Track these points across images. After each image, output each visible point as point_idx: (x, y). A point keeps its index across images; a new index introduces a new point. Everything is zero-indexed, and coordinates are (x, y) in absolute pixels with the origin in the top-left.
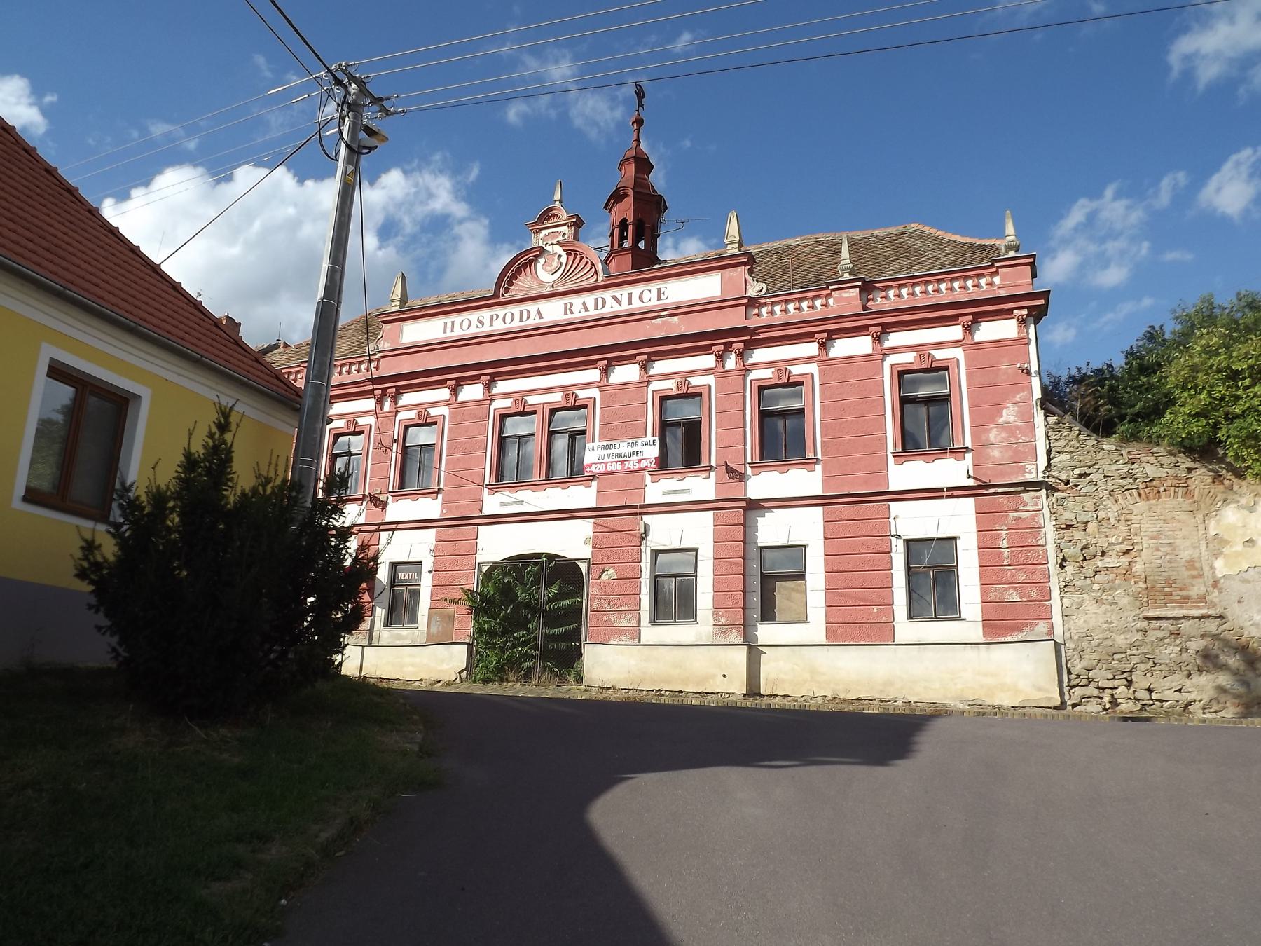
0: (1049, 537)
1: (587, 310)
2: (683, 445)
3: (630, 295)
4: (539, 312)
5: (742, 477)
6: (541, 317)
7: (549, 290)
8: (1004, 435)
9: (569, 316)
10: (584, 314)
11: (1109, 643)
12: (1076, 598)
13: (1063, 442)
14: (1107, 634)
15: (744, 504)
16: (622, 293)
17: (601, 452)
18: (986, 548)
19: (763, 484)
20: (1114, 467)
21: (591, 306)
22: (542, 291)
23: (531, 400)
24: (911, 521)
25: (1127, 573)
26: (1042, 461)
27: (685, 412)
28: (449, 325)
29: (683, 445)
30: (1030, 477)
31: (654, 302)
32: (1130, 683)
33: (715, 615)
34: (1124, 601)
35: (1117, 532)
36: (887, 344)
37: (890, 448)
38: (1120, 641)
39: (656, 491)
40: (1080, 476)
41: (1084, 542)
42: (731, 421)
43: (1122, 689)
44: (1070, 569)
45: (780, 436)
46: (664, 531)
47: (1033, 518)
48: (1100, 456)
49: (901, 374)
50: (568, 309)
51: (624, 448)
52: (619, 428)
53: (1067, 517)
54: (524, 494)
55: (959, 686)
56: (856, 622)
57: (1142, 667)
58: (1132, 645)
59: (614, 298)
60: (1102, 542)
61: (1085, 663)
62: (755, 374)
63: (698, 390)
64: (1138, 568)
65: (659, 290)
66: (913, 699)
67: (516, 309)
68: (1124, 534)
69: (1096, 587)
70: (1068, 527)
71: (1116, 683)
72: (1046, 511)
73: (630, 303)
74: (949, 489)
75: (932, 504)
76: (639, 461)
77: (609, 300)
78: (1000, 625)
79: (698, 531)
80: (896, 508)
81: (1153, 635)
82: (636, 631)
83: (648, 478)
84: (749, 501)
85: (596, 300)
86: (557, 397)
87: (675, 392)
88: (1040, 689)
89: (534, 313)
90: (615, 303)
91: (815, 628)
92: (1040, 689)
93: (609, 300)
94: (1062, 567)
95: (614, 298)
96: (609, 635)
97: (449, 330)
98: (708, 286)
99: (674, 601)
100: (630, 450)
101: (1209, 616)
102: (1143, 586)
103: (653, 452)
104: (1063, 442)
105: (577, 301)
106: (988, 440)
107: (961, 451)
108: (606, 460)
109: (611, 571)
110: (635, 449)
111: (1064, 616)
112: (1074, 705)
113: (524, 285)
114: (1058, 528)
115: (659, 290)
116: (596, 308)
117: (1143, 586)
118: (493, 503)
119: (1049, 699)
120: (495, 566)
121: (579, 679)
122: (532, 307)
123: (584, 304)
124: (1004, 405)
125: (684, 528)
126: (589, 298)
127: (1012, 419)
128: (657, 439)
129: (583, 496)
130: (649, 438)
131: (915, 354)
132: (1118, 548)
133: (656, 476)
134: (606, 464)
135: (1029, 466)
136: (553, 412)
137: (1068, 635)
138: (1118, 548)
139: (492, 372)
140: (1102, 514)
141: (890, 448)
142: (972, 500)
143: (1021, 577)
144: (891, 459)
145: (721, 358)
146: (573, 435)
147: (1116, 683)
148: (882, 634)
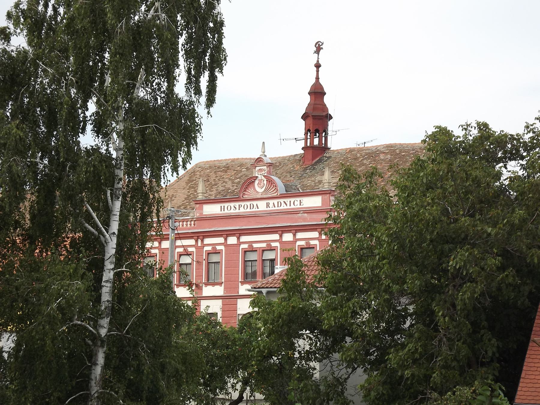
6: (258, 208)
9: (268, 209)
10: (274, 208)
16: (287, 200)
21: (276, 205)
22: (259, 196)
23: (255, 246)
28: (223, 208)
31: (299, 206)
36: (241, 241)
49: (208, 254)
50: (268, 205)
59: (284, 202)
62: (299, 243)
63: (313, 246)
67: (248, 203)
77: (283, 203)
80: (239, 301)
86: (264, 245)
90: (285, 205)
93: (283, 203)
95: (284, 202)
97: (223, 210)
105: (271, 202)
113: (251, 192)
122: (255, 203)
126: (275, 201)
131: (266, 244)
136: (263, 251)
139: (239, 233)
142: (221, 300)
145: (320, 234)
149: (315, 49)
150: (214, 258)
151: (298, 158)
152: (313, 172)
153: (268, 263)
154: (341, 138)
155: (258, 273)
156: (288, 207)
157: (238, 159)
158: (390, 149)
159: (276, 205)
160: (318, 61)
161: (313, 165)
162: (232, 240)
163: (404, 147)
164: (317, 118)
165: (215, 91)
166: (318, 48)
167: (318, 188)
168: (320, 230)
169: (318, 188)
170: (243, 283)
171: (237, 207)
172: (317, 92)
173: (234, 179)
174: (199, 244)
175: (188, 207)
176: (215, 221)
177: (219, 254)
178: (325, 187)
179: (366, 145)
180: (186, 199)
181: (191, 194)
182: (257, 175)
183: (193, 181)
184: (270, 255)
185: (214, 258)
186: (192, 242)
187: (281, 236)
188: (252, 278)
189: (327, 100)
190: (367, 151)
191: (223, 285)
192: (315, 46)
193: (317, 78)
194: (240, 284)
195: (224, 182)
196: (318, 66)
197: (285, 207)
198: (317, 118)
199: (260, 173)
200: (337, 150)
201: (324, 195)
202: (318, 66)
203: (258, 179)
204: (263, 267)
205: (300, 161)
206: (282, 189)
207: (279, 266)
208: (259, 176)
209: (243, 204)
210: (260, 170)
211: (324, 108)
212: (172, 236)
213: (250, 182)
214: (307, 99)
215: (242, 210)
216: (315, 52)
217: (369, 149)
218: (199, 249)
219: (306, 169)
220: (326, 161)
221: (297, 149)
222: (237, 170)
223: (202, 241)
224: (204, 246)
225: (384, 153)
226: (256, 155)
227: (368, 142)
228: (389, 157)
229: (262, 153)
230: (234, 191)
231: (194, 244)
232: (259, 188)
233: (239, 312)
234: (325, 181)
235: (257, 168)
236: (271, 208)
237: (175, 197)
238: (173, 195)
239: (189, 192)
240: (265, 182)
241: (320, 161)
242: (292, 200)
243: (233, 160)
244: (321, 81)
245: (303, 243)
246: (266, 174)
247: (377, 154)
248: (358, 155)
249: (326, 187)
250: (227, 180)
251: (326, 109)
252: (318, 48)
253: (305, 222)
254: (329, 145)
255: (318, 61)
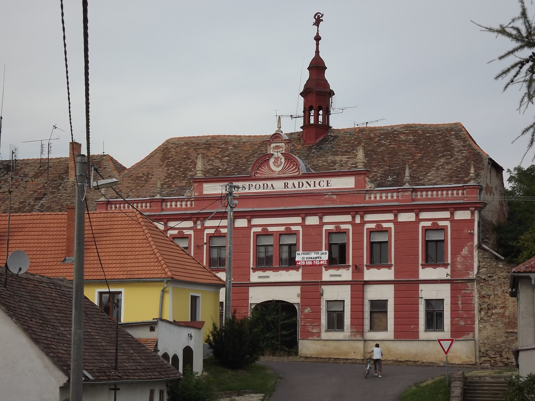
0: (476, 300)
1: (295, 187)
2: (338, 258)
3: (315, 182)
4: (272, 185)
5: (362, 272)
7: (277, 176)
8: (463, 259)
11: (494, 341)
12: (484, 324)
13: (484, 264)
14: (493, 338)
15: (362, 283)
16: (311, 181)
17: (303, 256)
18: (454, 303)
19: (370, 274)
20: (502, 274)
21: (297, 186)
22: (274, 175)
23: (270, 229)
24: (427, 292)
25: (503, 315)
26: (476, 270)
27: (337, 239)
29: (338, 258)
30: (471, 277)
32: (501, 356)
33: (351, 328)
34: (501, 326)
35: (500, 299)
37: (420, 262)
38: (498, 340)
39: (327, 275)
40: (490, 277)
41: (489, 303)
42: (358, 247)
43: (498, 358)
44: (483, 313)
45: (378, 256)
46: (330, 293)
47: (471, 293)
48: (497, 269)
50: (286, 185)
51: (313, 255)
52: (312, 245)
53: (483, 293)
54: (268, 273)
55: (441, 356)
56: (406, 331)
57: (506, 350)
58: (503, 342)
59: (307, 182)
60: (495, 303)
61: (485, 349)
63: (345, 231)
64: (507, 314)
65: (327, 181)
66: (425, 361)
67: (261, 183)
68: (503, 300)
69: (491, 320)
70: (483, 297)
71: (496, 356)
72: (476, 290)
73: (315, 186)
74: (440, 280)
75: (434, 285)
76: (320, 261)
77: (305, 183)
78: (458, 332)
79: (344, 293)
81: (510, 338)
82: (319, 334)
83: (324, 269)
84: (365, 281)
85: (299, 183)
86: (282, 229)
87: (335, 231)
88: (468, 358)
89: (270, 186)
91: (390, 334)
92: (468, 358)
93: (305, 183)
94: (480, 312)
95: (307, 182)
96: (307, 335)
98: (347, 183)
99: (336, 322)
100: (316, 256)
101: (356, 363)
102: (508, 320)
103: (326, 257)
104: (484, 264)
105: (290, 182)
106: (457, 261)
107: (445, 266)
108: (305, 260)
109: (309, 309)
110: (318, 256)
111: (479, 331)
112: (480, 364)
113: (264, 171)
114: (480, 297)
115: (327, 181)
116: (299, 187)
117: (508, 320)
118: (255, 277)
119: (471, 361)
120: (258, 305)
121: (296, 353)
122: (269, 183)
123: (293, 184)
124: (463, 247)
125: (336, 291)
126: (296, 182)
127: (466, 253)
128: (327, 252)
129: (296, 276)
130: (324, 251)
132: (500, 305)
133: (327, 268)
134: (305, 261)
135: (471, 273)
136: (280, 235)
137: (480, 338)
138: (500, 305)
140: (496, 292)
141: (420, 262)
143: (465, 316)
144: (420, 267)
146: (290, 246)
147: (496, 356)
148: (413, 336)
149: (314, 21)
150: (217, 242)
151: (296, 136)
152: (321, 152)
153: (285, 249)
154: (342, 118)
155: (274, 259)
156: (312, 188)
157: (219, 136)
158: (409, 129)
159: (297, 186)
160: (318, 34)
161: (317, 145)
162: (312, 220)
163: (426, 128)
164: (317, 93)
165: (88, 69)
166: (318, 21)
167: (335, 169)
168: (354, 213)
169: (335, 169)
170: (254, 270)
171: (247, 187)
172: (317, 67)
173: (222, 157)
174: (199, 227)
175: (173, 186)
176: (291, 199)
177: (344, 234)
178: (198, 175)
179: (369, 125)
180: (166, 177)
181: (172, 172)
182: (272, 152)
183: (169, 158)
184: (291, 240)
185: (217, 242)
186: (190, 224)
187: (304, 219)
188: (267, 264)
189: (328, 75)
190: (382, 132)
191: (393, 268)
192: (315, 17)
193: (317, 52)
194: (251, 271)
195: (210, 160)
196: (318, 39)
197: (309, 188)
198: (317, 93)
199: (277, 151)
200: (343, 129)
201: (357, 176)
202: (318, 39)
203: (273, 157)
204: (280, 252)
205: (300, 139)
206: (303, 170)
207: (301, 252)
208: (275, 154)
209: (254, 183)
210: (277, 147)
211: (326, 84)
212: (230, 214)
213: (265, 159)
214: (306, 75)
215: (253, 190)
216: (315, 24)
217: (384, 129)
218: (199, 233)
219: (310, 148)
220: (333, 140)
221: (294, 126)
222: (221, 148)
223: (362, 218)
224: (204, 228)
225: (404, 133)
226: (271, 132)
227: (372, 122)
228: (411, 137)
229: (277, 129)
230: (225, 169)
231: (350, 220)
232: (275, 167)
233: (251, 301)
234: (359, 161)
235: (273, 145)
236: (290, 188)
237: (153, 175)
238: (148, 173)
239: (168, 170)
240: (283, 160)
241: (324, 141)
242: (317, 180)
243: (214, 137)
244: (321, 55)
245: (332, 227)
246: (283, 152)
247: (396, 134)
248: (372, 135)
249: (361, 167)
250: (213, 158)
251: (327, 85)
252: (318, 21)
253: (334, 204)
254: (331, 125)
255: (318, 34)
